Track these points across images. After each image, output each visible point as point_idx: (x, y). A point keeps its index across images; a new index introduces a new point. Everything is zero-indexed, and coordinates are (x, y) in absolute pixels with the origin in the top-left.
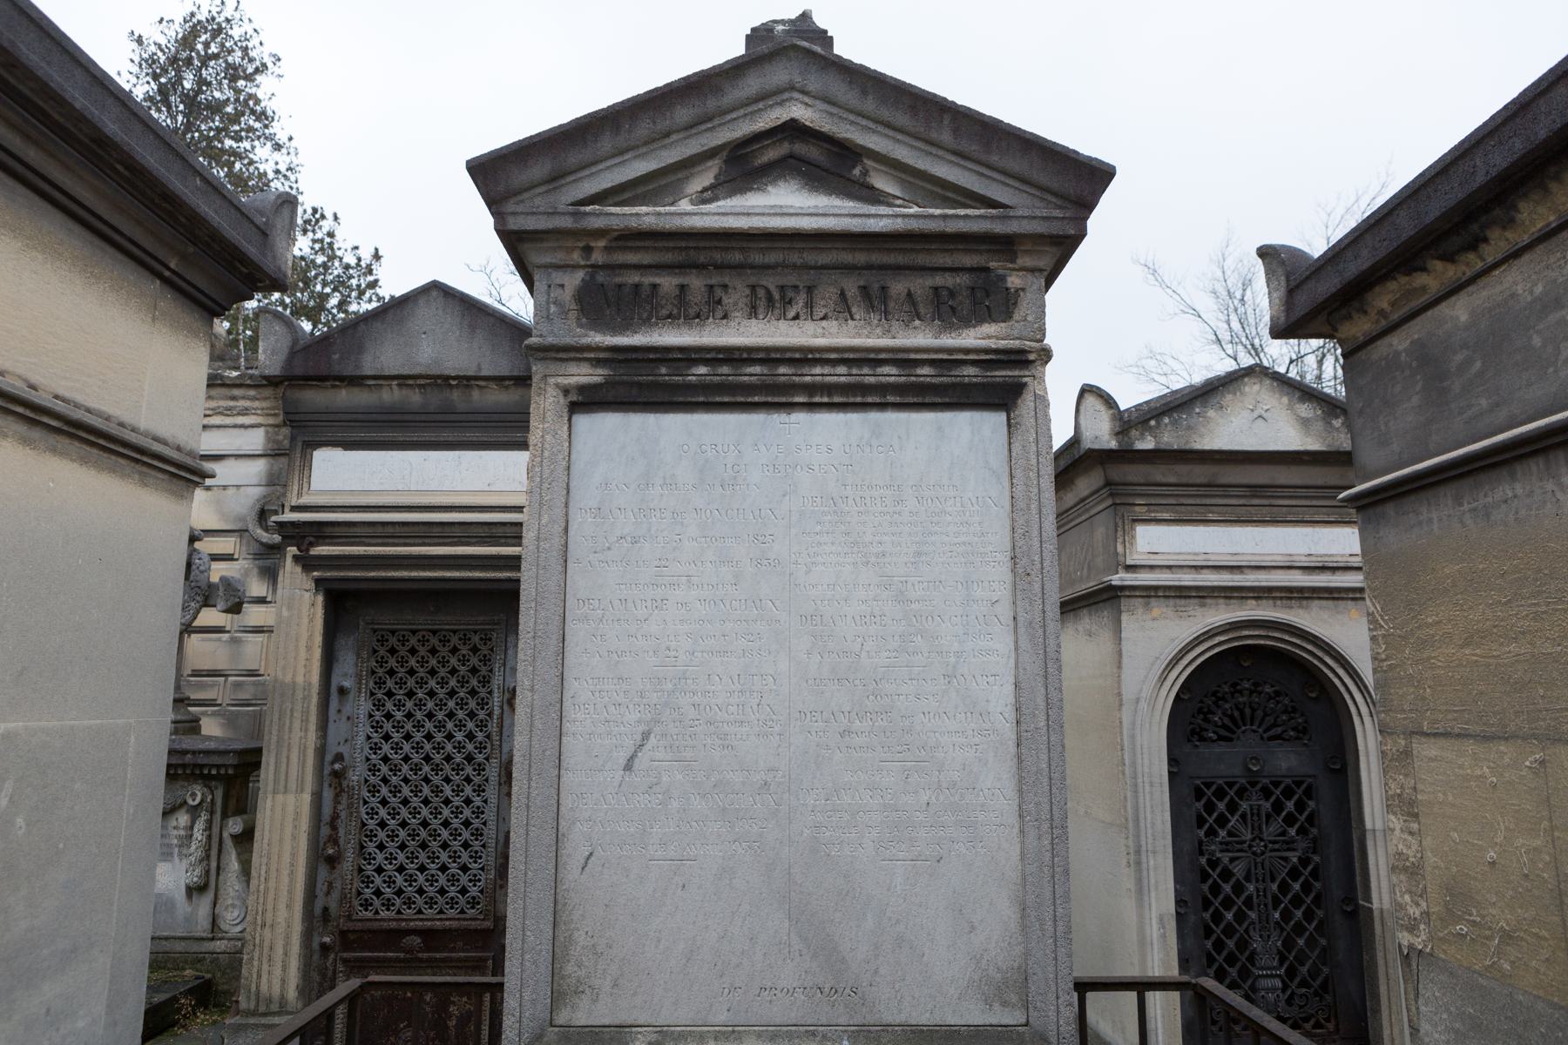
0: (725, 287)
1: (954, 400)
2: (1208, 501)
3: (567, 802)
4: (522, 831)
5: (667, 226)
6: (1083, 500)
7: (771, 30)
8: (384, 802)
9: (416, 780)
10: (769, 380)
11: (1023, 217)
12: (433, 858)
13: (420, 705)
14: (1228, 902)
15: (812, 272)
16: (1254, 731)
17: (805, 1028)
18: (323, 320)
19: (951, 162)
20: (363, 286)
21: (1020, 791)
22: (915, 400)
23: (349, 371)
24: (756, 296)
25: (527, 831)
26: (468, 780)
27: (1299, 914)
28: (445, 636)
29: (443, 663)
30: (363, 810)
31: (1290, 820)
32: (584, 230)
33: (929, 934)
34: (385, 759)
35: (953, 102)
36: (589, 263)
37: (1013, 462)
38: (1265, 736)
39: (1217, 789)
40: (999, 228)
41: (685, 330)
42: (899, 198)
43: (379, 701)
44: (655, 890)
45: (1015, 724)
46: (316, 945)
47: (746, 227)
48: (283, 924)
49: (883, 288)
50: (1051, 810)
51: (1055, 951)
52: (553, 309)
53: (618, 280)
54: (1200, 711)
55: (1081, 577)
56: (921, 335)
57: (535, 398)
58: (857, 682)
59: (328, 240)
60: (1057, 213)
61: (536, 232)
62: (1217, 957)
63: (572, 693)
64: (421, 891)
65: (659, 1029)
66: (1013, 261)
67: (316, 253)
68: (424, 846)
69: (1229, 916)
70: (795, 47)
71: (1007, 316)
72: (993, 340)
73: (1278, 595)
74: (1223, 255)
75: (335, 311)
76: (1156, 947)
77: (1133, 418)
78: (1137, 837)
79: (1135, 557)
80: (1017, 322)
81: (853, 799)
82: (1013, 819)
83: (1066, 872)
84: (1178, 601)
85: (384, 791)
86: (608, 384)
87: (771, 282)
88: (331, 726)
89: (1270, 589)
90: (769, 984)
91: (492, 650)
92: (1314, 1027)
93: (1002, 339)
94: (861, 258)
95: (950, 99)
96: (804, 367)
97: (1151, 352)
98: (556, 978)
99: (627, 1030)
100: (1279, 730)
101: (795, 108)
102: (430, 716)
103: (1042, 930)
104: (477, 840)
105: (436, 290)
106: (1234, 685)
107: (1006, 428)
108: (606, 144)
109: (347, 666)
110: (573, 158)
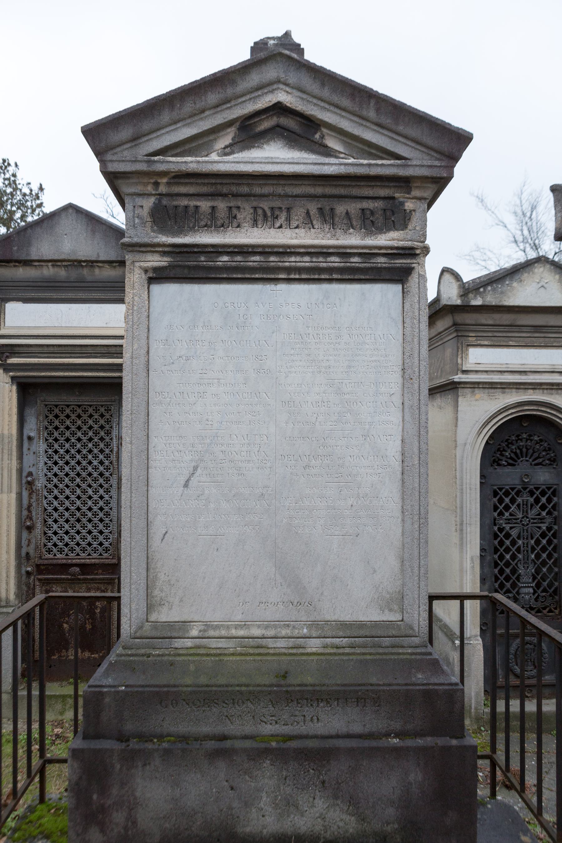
0: (238, 208)
1: (372, 277)
2: (510, 335)
3: (153, 505)
4: (128, 520)
5: (204, 170)
6: (440, 333)
7: (266, 44)
8: (56, 498)
9: (72, 486)
10: (265, 265)
11: (416, 166)
12: (84, 527)
13: (73, 446)
14: (507, 550)
15: (290, 199)
16: (527, 461)
17: (284, 623)
18: (13, 226)
19: (374, 130)
20: (34, 206)
21: (403, 499)
22: (350, 277)
23: (23, 257)
24: (257, 214)
25: (131, 520)
26: (101, 486)
27: (544, 556)
28: (85, 408)
29: (85, 423)
30: (45, 502)
31: (543, 507)
32: (154, 172)
33: (351, 575)
34: (56, 475)
35: (377, 92)
36: (157, 192)
37: (405, 314)
38: (533, 463)
39: (505, 491)
40: (401, 172)
41: (215, 234)
42: (342, 153)
43: (51, 443)
44: (202, 551)
45: (401, 462)
46: (23, 572)
47: (251, 171)
48: (5, 561)
49: (332, 209)
50: (420, 509)
51: (419, 584)
52: (137, 221)
53: (175, 203)
54: (499, 450)
55: (437, 376)
56: (354, 238)
57: (127, 275)
58: (314, 439)
59: (12, 179)
60: (437, 163)
61: (124, 173)
62: (500, 577)
63: (153, 445)
64: (78, 544)
65: (205, 623)
66: (409, 193)
67: (6, 186)
68: (78, 521)
69: (508, 557)
70: (281, 54)
71: (404, 226)
72: (396, 241)
73: (545, 387)
74: (521, 191)
75: (19, 221)
76: (468, 573)
77: (470, 287)
78: (462, 516)
79: (468, 365)
80: (410, 230)
81: (310, 503)
82: (398, 514)
83: (427, 542)
84: (490, 390)
85: (56, 492)
86: (171, 267)
87: (265, 205)
88: (25, 456)
89: (541, 384)
90: (264, 601)
91: (111, 416)
92: (548, 612)
93: (401, 241)
94: (319, 190)
95: (375, 89)
96: (284, 257)
97: (478, 247)
98: (149, 597)
99: (188, 624)
100: (541, 460)
101: (280, 95)
102: (79, 452)
103: (412, 572)
104: (107, 517)
105: (71, 208)
106: (518, 436)
107: (401, 294)
108: (166, 116)
109: (31, 428)
110: (146, 126)
